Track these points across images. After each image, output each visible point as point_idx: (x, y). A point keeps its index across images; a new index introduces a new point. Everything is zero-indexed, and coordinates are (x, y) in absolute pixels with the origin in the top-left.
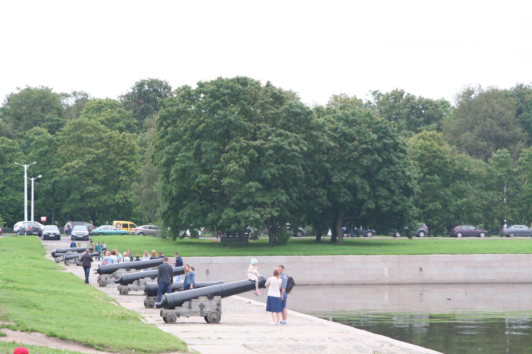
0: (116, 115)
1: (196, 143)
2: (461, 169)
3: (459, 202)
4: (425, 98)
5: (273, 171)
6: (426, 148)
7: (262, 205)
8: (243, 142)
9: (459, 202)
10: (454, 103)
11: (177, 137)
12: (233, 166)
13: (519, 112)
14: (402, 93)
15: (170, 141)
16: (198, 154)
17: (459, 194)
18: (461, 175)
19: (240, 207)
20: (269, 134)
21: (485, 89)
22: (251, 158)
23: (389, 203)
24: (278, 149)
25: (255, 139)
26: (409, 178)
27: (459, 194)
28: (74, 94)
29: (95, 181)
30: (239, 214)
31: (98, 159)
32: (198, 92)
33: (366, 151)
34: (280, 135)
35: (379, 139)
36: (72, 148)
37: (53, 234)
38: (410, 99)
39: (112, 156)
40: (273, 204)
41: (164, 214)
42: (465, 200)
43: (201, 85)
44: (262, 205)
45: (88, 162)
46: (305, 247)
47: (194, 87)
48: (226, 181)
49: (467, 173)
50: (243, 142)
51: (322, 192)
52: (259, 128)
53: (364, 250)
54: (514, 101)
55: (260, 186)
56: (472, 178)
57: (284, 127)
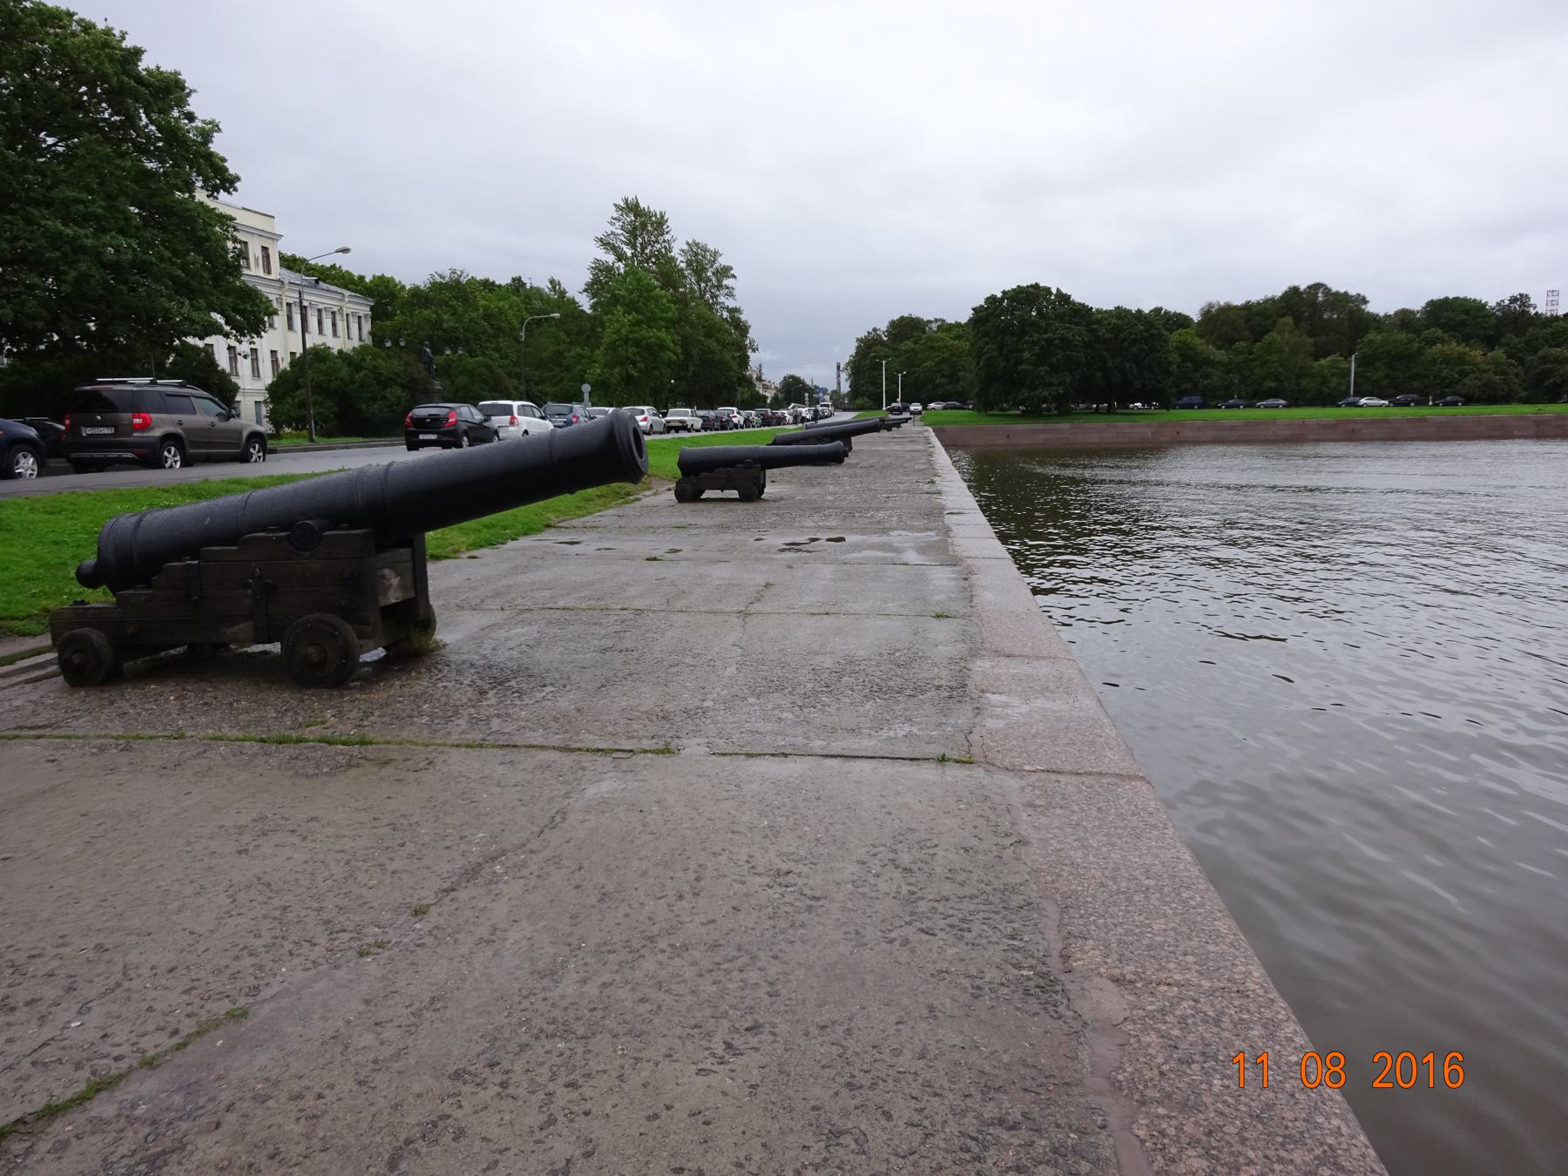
0: (961, 333)
2: (1208, 357)
3: (1206, 382)
4: (1173, 311)
5: (1059, 357)
6: (1180, 342)
7: (1051, 384)
8: (1036, 337)
10: (1196, 317)
11: (986, 334)
12: (1026, 355)
13: (1247, 321)
14: (1161, 309)
15: (980, 338)
16: (1001, 348)
17: (1207, 376)
18: (1208, 362)
20: (1057, 329)
21: (1222, 303)
23: (1154, 382)
24: (1063, 339)
25: (1046, 332)
26: (1170, 363)
27: (1207, 376)
28: (936, 320)
29: (943, 376)
30: (1032, 394)
31: (944, 360)
32: (1002, 299)
33: (1135, 340)
34: (1067, 328)
35: (1147, 330)
38: (1167, 313)
39: (954, 358)
40: (1059, 384)
41: (978, 393)
42: (1209, 381)
43: (1004, 293)
44: (1051, 384)
45: (938, 362)
46: (1084, 417)
47: (999, 295)
48: (1021, 368)
49: (1213, 360)
50: (1036, 337)
51: (1099, 374)
52: (1050, 325)
53: (104, 602)
54: (1245, 312)
55: (1049, 369)
56: (1213, 364)
57: (1070, 322)
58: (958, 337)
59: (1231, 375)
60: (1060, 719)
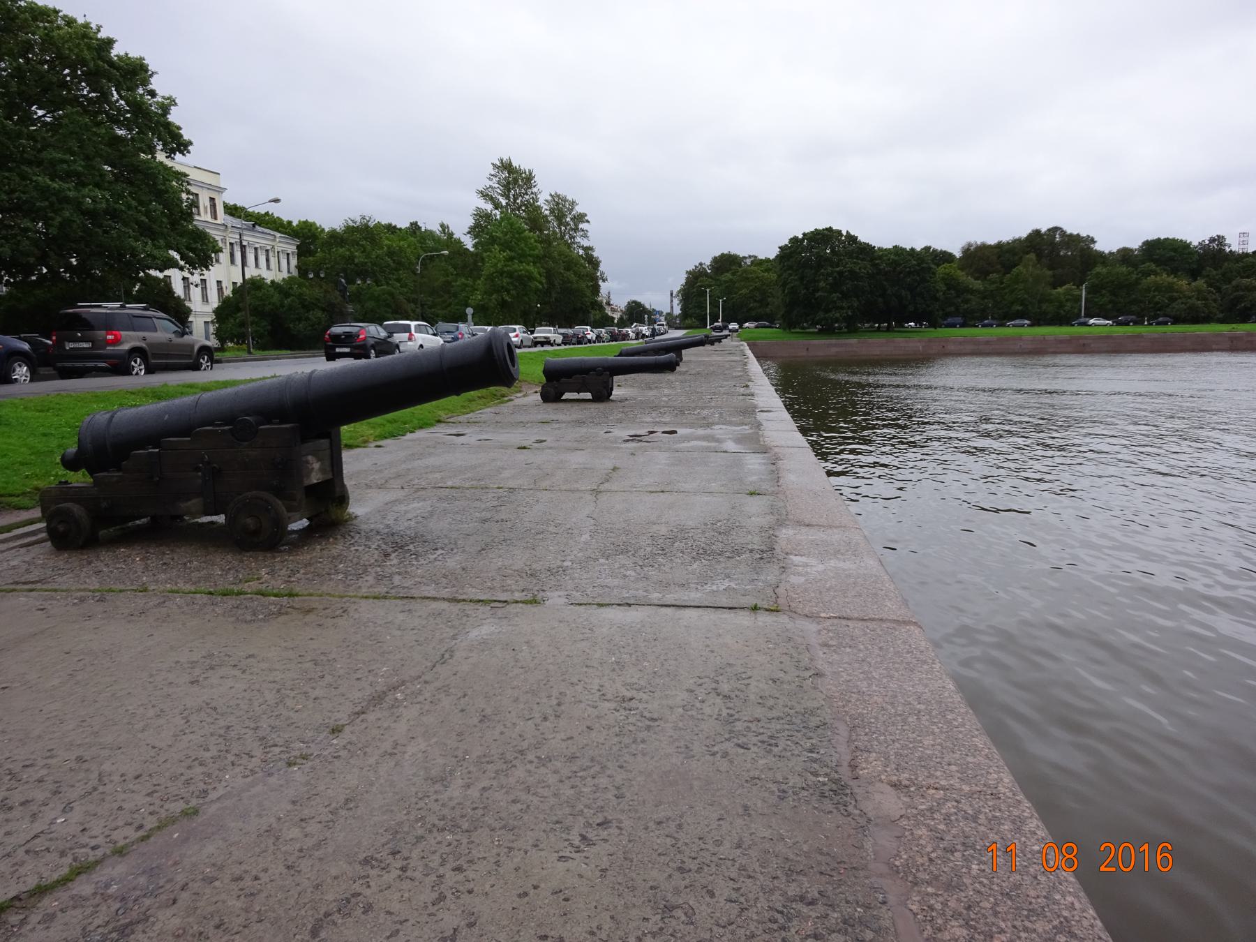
0: (770, 267)
1: (800, 271)
2: (968, 286)
3: (966, 306)
4: (939, 249)
5: (848, 286)
6: (945, 274)
7: (842, 308)
8: (830, 270)
9: (966, 306)
10: (958, 254)
11: (790, 268)
12: (822, 284)
13: (999, 257)
14: (930, 248)
15: (785, 271)
16: (802, 279)
17: (967, 301)
18: (968, 290)
19: (828, 311)
20: (847, 263)
21: (979, 243)
22: (835, 278)
23: (924, 306)
24: (852, 272)
25: (838, 266)
26: (937, 291)
27: (967, 301)
28: (750, 257)
29: (755, 301)
30: (827, 315)
31: (756, 289)
32: (803, 239)
33: (910, 273)
34: (855, 263)
35: (919, 265)
36: (742, 284)
37: (1073, 325)
38: (935, 251)
39: (764, 287)
40: (849, 308)
41: (783, 315)
42: (969, 305)
43: (804, 234)
44: (842, 308)
45: (752, 290)
46: (868, 334)
47: (800, 236)
48: (818, 295)
49: (971, 289)
50: (830, 270)
51: (880, 300)
52: (841, 260)
54: (997, 250)
55: (840, 296)
56: (972, 291)
57: (857, 258)
58: (767, 270)
59: (986, 301)
60: (849, 576)
